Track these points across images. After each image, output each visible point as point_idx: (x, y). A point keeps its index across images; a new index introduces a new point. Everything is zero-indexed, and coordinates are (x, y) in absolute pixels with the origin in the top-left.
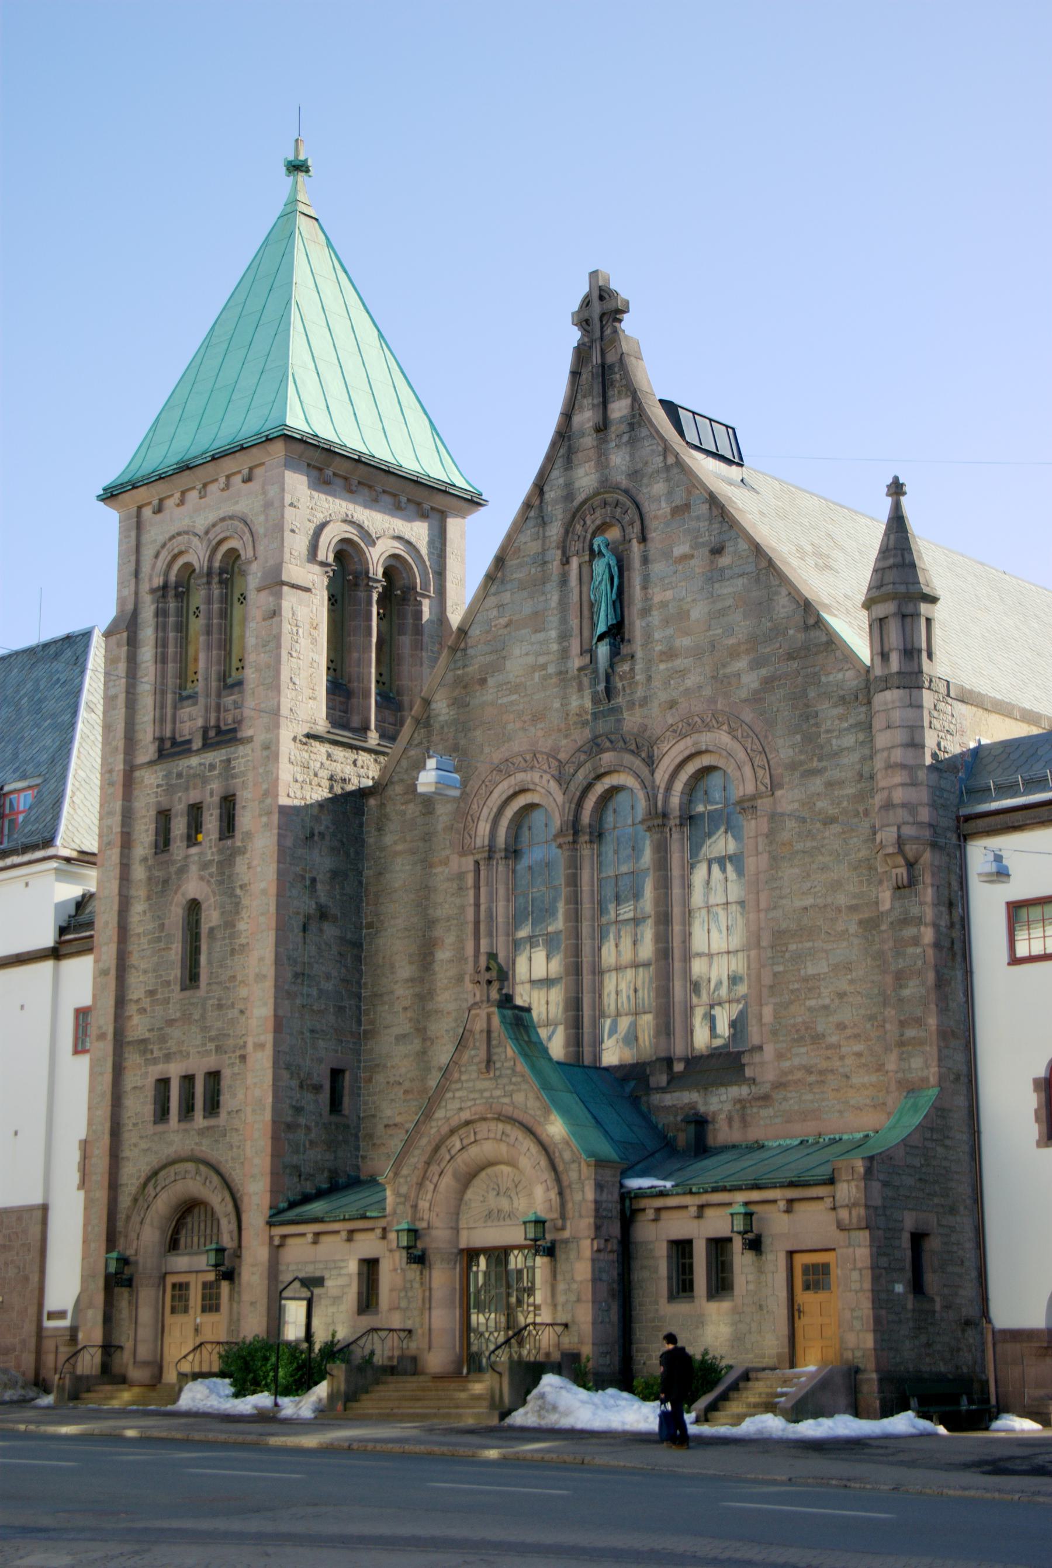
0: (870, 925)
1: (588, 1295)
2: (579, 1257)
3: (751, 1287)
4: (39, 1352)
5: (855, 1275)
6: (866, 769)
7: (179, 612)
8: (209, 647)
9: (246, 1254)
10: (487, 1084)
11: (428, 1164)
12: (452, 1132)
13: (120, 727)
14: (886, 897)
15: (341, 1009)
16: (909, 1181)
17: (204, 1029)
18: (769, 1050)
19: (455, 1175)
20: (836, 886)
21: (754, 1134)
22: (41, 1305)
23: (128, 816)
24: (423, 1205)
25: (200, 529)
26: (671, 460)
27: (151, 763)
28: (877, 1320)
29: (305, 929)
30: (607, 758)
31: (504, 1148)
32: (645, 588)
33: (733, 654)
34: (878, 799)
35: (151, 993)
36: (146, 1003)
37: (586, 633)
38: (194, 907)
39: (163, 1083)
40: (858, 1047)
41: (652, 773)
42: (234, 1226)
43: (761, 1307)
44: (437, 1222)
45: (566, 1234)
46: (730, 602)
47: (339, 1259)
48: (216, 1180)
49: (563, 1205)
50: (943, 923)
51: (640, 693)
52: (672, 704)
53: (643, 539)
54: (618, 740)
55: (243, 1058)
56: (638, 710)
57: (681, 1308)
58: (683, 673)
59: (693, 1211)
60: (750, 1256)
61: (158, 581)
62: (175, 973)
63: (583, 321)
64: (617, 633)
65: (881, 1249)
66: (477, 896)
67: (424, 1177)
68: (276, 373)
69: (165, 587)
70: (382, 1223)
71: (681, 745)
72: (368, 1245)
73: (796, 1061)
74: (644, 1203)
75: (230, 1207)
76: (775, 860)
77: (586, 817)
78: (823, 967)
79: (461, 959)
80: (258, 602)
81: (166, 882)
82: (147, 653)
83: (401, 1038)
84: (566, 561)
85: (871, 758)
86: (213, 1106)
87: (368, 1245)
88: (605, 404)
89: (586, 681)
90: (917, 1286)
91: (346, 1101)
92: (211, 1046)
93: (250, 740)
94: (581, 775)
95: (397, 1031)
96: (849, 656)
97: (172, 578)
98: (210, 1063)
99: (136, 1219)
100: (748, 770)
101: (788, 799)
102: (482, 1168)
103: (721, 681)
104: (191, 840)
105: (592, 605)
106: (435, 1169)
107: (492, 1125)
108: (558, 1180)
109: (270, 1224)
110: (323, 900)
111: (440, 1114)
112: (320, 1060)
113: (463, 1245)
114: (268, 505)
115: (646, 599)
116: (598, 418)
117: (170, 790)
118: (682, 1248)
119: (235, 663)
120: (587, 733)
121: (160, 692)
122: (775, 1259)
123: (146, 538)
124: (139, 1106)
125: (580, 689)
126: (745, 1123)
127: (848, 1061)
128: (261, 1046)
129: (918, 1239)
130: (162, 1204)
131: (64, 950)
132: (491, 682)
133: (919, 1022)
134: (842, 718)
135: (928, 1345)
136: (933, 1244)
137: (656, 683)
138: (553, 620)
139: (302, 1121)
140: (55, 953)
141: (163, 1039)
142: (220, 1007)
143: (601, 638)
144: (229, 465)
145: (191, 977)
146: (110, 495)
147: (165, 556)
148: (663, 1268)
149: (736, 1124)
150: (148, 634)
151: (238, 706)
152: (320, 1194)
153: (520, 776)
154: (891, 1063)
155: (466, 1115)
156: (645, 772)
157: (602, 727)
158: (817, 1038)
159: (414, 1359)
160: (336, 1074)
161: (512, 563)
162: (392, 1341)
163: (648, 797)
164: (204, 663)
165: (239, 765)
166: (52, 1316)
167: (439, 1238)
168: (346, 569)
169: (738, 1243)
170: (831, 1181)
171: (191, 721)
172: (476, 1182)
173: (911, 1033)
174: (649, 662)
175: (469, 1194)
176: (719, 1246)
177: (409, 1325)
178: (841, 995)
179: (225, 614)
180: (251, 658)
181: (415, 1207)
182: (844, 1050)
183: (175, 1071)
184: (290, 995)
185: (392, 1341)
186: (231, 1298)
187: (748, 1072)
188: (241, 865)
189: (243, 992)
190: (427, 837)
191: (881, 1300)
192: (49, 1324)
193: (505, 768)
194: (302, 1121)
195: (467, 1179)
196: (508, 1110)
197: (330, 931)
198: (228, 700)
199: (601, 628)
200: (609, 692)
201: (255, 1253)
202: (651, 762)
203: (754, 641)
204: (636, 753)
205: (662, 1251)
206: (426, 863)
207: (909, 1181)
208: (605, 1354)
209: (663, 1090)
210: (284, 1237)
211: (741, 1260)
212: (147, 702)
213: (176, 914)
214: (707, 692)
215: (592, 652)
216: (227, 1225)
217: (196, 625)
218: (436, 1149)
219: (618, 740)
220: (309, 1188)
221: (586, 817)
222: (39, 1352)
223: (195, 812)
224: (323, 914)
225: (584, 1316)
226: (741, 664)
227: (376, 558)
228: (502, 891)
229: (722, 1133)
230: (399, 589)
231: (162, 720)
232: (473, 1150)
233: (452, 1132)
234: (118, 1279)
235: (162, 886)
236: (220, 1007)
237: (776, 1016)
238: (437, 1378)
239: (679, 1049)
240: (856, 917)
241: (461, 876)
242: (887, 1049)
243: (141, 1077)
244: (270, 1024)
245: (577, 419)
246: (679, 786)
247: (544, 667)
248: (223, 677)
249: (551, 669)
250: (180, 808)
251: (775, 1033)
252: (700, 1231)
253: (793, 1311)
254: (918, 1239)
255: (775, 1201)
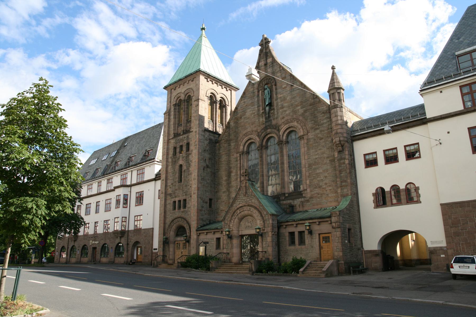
0: (333, 161)
1: (271, 245)
2: (268, 236)
3: (310, 242)
4: (152, 256)
5: (337, 239)
6: (330, 127)
7: (179, 109)
8: (184, 115)
9: (192, 237)
10: (245, 198)
11: (232, 216)
12: (238, 209)
13: (167, 131)
14: (336, 154)
15: (211, 187)
16: (347, 217)
17: (183, 191)
18: (308, 190)
19: (238, 219)
20: (323, 153)
21: (305, 208)
22: (152, 247)
23: (168, 149)
24: (231, 225)
25: (183, 92)
26: (281, 69)
27: (172, 138)
28: (343, 249)
29: (204, 169)
30: (269, 130)
31: (250, 212)
32: (276, 95)
33: (297, 106)
34: (333, 133)
35: (172, 184)
36: (171, 186)
37: (263, 105)
38: (181, 166)
39: (175, 202)
40: (330, 188)
41: (279, 132)
42: (189, 231)
43: (312, 247)
44: (234, 229)
45: (265, 231)
46: (296, 95)
47: (211, 237)
48: (185, 222)
49: (264, 224)
50: (350, 159)
51: (276, 116)
52: (283, 118)
53: (276, 85)
54: (271, 126)
55: (191, 196)
56: (275, 120)
57: (292, 248)
58: (285, 111)
59: (295, 225)
60: (309, 236)
61: (174, 103)
62: (177, 180)
63: (261, 45)
64: (270, 105)
65: (343, 232)
66: (240, 162)
67: (231, 219)
68: (198, 61)
69: (176, 104)
70: (221, 230)
71: (286, 126)
72: (218, 235)
73: (315, 192)
74: (282, 224)
75: (188, 227)
76: (308, 149)
77: (264, 143)
78: (321, 171)
79: (237, 175)
80: (194, 103)
81: (175, 161)
82: (172, 117)
83: (224, 192)
84: (258, 92)
85: (331, 124)
86: (185, 207)
87: (218, 235)
88: (266, 60)
89: (264, 115)
90: (349, 241)
91: (212, 205)
92: (184, 194)
93: (192, 131)
94: (263, 135)
95: (223, 191)
96: (325, 103)
97: (177, 102)
98: (184, 197)
99: (169, 230)
100: (301, 130)
101: (311, 135)
102: (245, 217)
103: (295, 112)
104: (180, 153)
105: (264, 99)
106: (234, 217)
107: (247, 207)
108: (263, 219)
109: (197, 231)
110: (208, 164)
111: (235, 205)
112: (207, 197)
113: (240, 234)
114: (196, 85)
115: (277, 97)
116: (265, 62)
117: (176, 143)
118: (292, 234)
119: (190, 117)
120: (264, 126)
121: (174, 124)
122: (316, 237)
123: (172, 95)
124: (170, 207)
125: (262, 117)
126: (303, 206)
127: (328, 191)
128: (194, 193)
129: (349, 230)
130: (174, 227)
131: (157, 179)
132: (243, 117)
133: (345, 181)
134: (323, 116)
135: (352, 254)
136: (352, 231)
137: (279, 114)
138: (256, 104)
139: (203, 209)
140: (155, 180)
141: (174, 193)
142: (186, 186)
143: (267, 105)
144: (189, 78)
145: (180, 181)
146: (165, 88)
147: (176, 98)
148: (287, 239)
149: (301, 206)
150: (172, 113)
151: (190, 125)
152: (207, 225)
153: (250, 136)
154: (339, 191)
155: (241, 205)
156: (277, 132)
157: (267, 124)
158: (320, 187)
159: (230, 259)
160: (211, 200)
161: (246, 94)
162: (224, 255)
163: (278, 138)
164: (183, 117)
165: (190, 137)
166: (155, 249)
167: (235, 232)
168: (212, 99)
169: (306, 232)
170: (330, 217)
171: (181, 129)
172: (243, 220)
173: (344, 184)
174: (278, 110)
175: (241, 223)
176: (301, 233)
177: (228, 252)
178: (326, 177)
179: (188, 108)
180: (193, 115)
181: (229, 226)
182: (327, 189)
183: (177, 199)
184: (201, 183)
185: (224, 255)
186: (189, 246)
187: (304, 195)
188: (190, 157)
189: (191, 183)
190: (229, 150)
191: (343, 244)
192: (154, 251)
193: (246, 135)
194: (203, 209)
195: (241, 219)
196: (251, 204)
197: (209, 170)
198: (188, 125)
199: (267, 103)
200: (269, 117)
201: (194, 236)
202: (279, 130)
203: (302, 102)
204: (275, 129)
205: (287, 234)
206: (229, 155)
207: (347, 217)
208: (274, 258)
209: (283, 200)
210: (200, 233)
211: (307, 236)
212: (172, 126)
213: (177, 167)
214: (291, 114)
215: (265, 109)
216: (188, 231)
217: (182, 111)
218: (234, 213)
219: (271, 126)
220: (205, 223)
221: (264, 143)
222: (152, 256)
223: (181, 147)
224: (207, 167)
225: (270, 250)
226: (299, 107)
227: (218, 99)
228: (245, 160)
229: (298, 209)
230: (223, 105)
231: (175, 130)
232: (242, 213)
233: (238, 209)
234: (165, 242)
235: (174, 162)
236: (186, 186)
237: (310, 182)
238: (235, 264)
239: (287, 191)
240: (329, 160)
241: (237, 158)
242: (338, 188)
243: (170, 201)
244: (196, 189)
245: (260, 64)
246: (285, 135)
247: (254, 113)
248: (187, 120)
249: (256, 114)
250: (178, 146)
251: (310, 186)
252: (296, 230)
253: (321, 248)
254: (349, 230)
255: (316, 222)
